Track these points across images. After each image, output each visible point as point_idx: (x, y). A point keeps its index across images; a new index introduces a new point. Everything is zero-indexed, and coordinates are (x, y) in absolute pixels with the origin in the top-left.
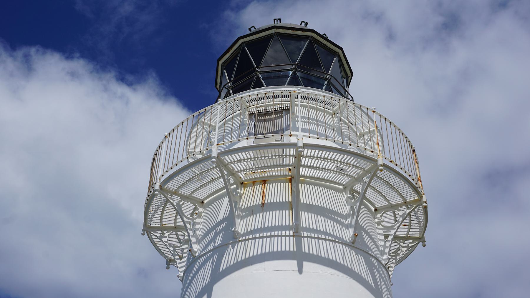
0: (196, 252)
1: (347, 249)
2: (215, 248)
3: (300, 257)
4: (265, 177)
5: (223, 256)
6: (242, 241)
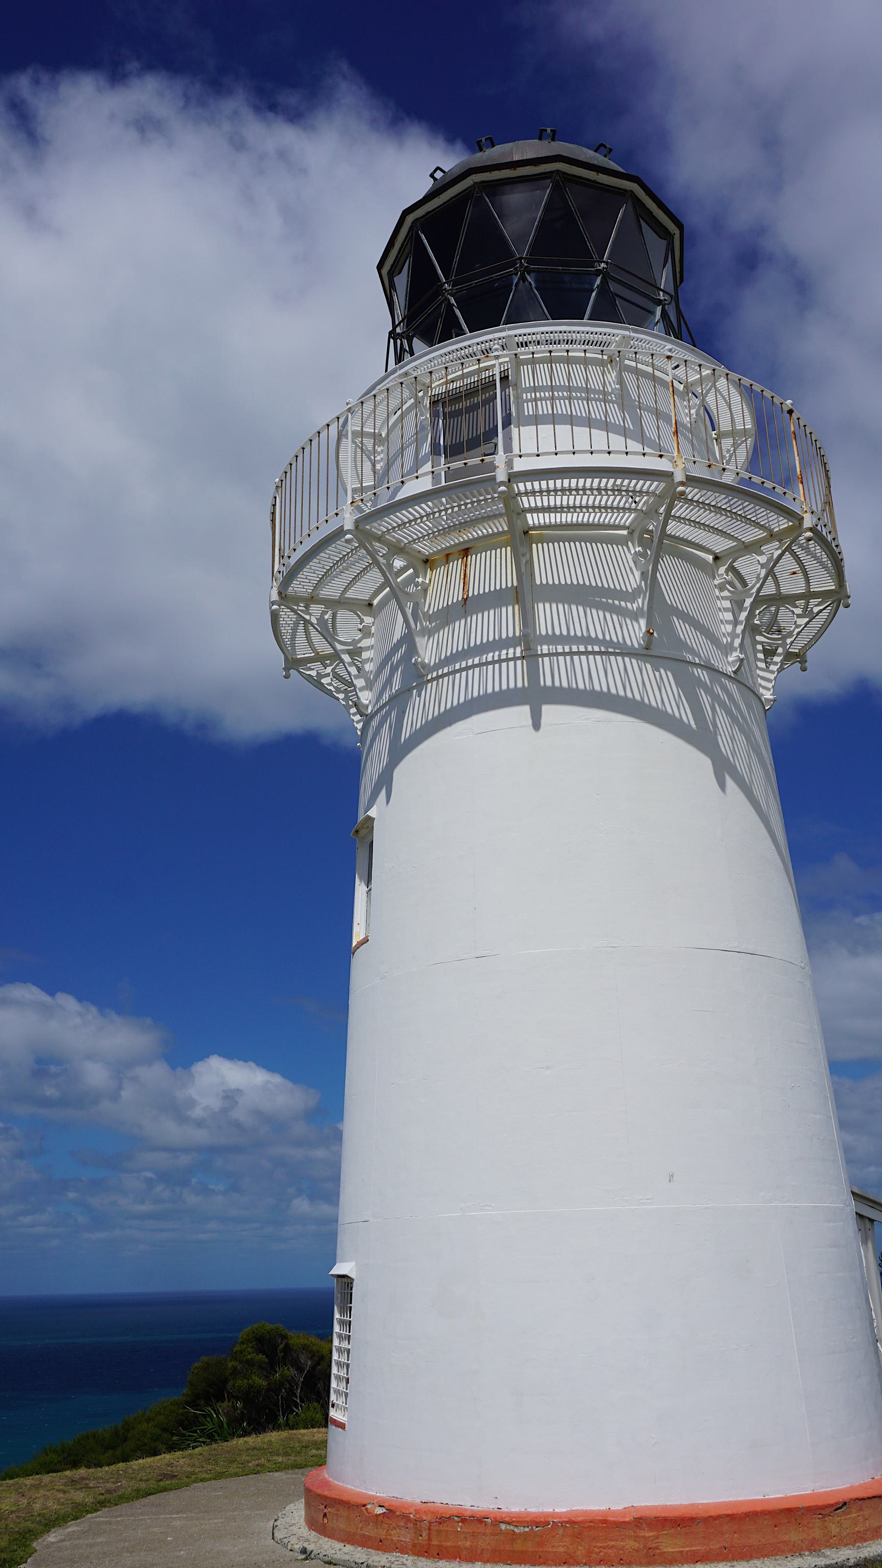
0: (367, 707)
1: (632, 664)
2: (392, 698)
3: (535, 697)
4: (465, 542)
5: (404, 712)
6: (433, 679)
